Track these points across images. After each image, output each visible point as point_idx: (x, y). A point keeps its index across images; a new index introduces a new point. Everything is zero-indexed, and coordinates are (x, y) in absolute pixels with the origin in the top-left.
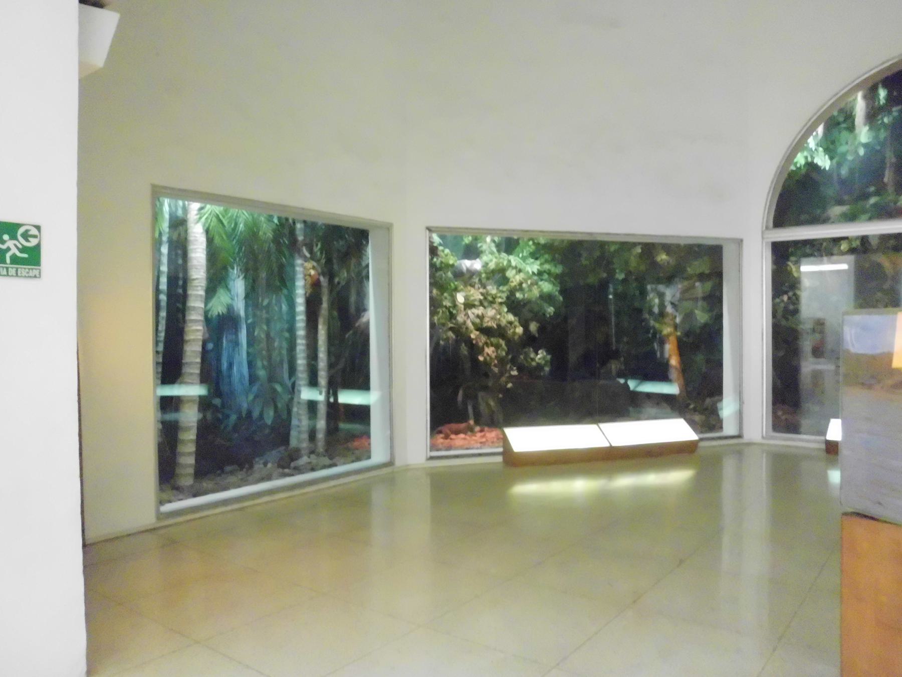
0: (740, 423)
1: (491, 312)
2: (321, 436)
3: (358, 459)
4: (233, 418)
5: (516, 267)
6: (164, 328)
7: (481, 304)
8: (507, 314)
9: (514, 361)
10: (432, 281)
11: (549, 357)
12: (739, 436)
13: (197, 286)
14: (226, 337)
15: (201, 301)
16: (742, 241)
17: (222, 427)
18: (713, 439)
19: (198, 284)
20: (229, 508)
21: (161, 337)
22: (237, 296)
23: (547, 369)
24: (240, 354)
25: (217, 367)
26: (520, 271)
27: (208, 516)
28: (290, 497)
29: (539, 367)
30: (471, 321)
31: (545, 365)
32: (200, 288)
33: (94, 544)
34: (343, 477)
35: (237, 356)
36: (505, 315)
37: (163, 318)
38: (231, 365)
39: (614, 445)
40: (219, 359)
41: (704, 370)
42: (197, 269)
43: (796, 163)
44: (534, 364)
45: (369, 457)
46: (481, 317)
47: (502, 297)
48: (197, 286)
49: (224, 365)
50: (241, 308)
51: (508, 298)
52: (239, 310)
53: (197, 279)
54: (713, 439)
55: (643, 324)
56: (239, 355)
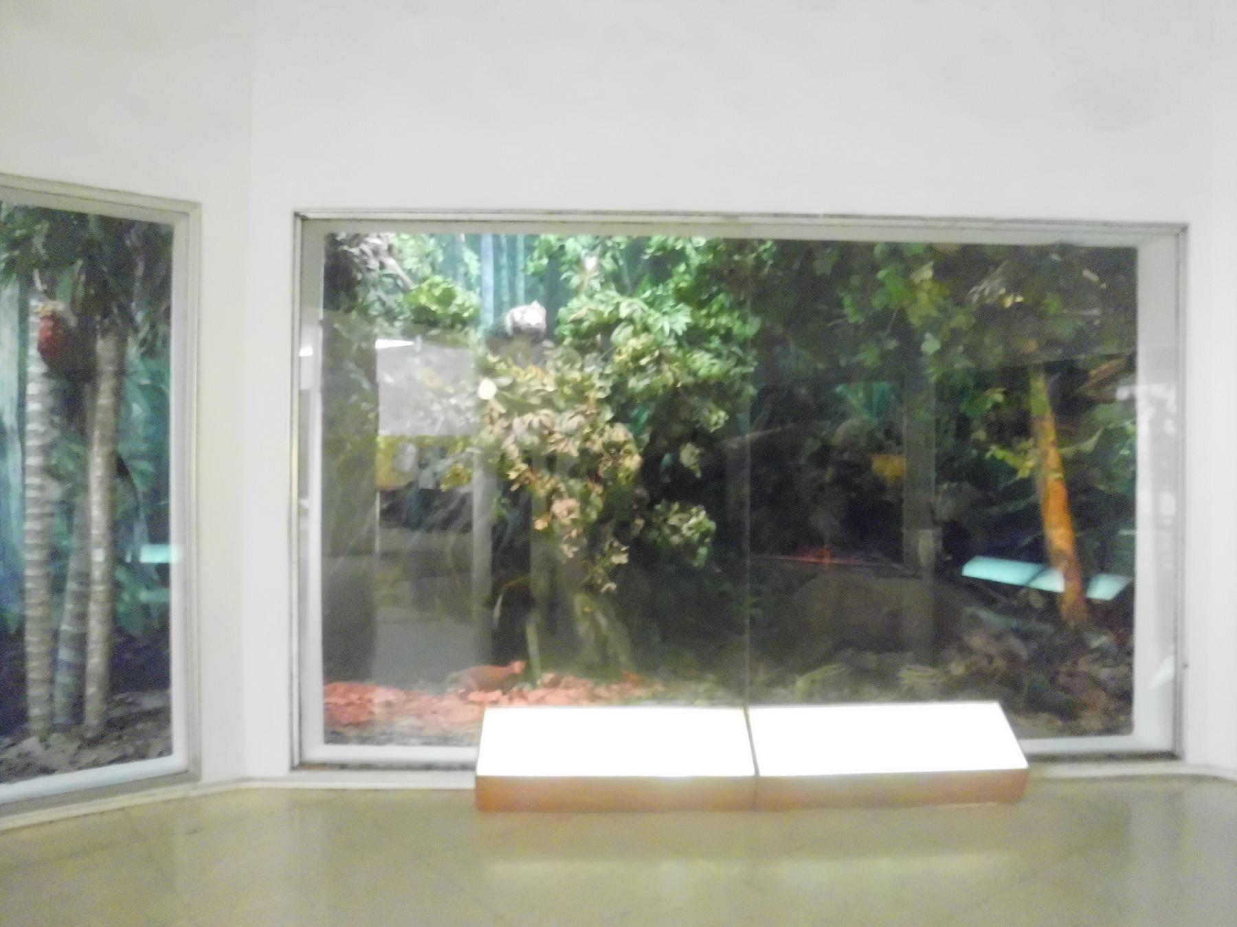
0: (1175, 705)
1: (569, 421)
2: (919, 674)
3: (141, 755)
5: (630, 320)
7: (548, 402)
8: (612, 426)
9: (622, 531)
10: (823, 266)
11: (712, 525)
12: (1170, 756)
16: (1184, 229)
18: (1112, 757)
23: (703, 551)
26: (646, 329)
29: (689, 548)
30: (516, 442)
31: (701, 542)
36: (607, 427)
39: (763, 773)
43: (12, 429)
44: (675, 539)
46: (545, 433)
47: (600, 388)
51: (615, 388)
54: (1112, 757)
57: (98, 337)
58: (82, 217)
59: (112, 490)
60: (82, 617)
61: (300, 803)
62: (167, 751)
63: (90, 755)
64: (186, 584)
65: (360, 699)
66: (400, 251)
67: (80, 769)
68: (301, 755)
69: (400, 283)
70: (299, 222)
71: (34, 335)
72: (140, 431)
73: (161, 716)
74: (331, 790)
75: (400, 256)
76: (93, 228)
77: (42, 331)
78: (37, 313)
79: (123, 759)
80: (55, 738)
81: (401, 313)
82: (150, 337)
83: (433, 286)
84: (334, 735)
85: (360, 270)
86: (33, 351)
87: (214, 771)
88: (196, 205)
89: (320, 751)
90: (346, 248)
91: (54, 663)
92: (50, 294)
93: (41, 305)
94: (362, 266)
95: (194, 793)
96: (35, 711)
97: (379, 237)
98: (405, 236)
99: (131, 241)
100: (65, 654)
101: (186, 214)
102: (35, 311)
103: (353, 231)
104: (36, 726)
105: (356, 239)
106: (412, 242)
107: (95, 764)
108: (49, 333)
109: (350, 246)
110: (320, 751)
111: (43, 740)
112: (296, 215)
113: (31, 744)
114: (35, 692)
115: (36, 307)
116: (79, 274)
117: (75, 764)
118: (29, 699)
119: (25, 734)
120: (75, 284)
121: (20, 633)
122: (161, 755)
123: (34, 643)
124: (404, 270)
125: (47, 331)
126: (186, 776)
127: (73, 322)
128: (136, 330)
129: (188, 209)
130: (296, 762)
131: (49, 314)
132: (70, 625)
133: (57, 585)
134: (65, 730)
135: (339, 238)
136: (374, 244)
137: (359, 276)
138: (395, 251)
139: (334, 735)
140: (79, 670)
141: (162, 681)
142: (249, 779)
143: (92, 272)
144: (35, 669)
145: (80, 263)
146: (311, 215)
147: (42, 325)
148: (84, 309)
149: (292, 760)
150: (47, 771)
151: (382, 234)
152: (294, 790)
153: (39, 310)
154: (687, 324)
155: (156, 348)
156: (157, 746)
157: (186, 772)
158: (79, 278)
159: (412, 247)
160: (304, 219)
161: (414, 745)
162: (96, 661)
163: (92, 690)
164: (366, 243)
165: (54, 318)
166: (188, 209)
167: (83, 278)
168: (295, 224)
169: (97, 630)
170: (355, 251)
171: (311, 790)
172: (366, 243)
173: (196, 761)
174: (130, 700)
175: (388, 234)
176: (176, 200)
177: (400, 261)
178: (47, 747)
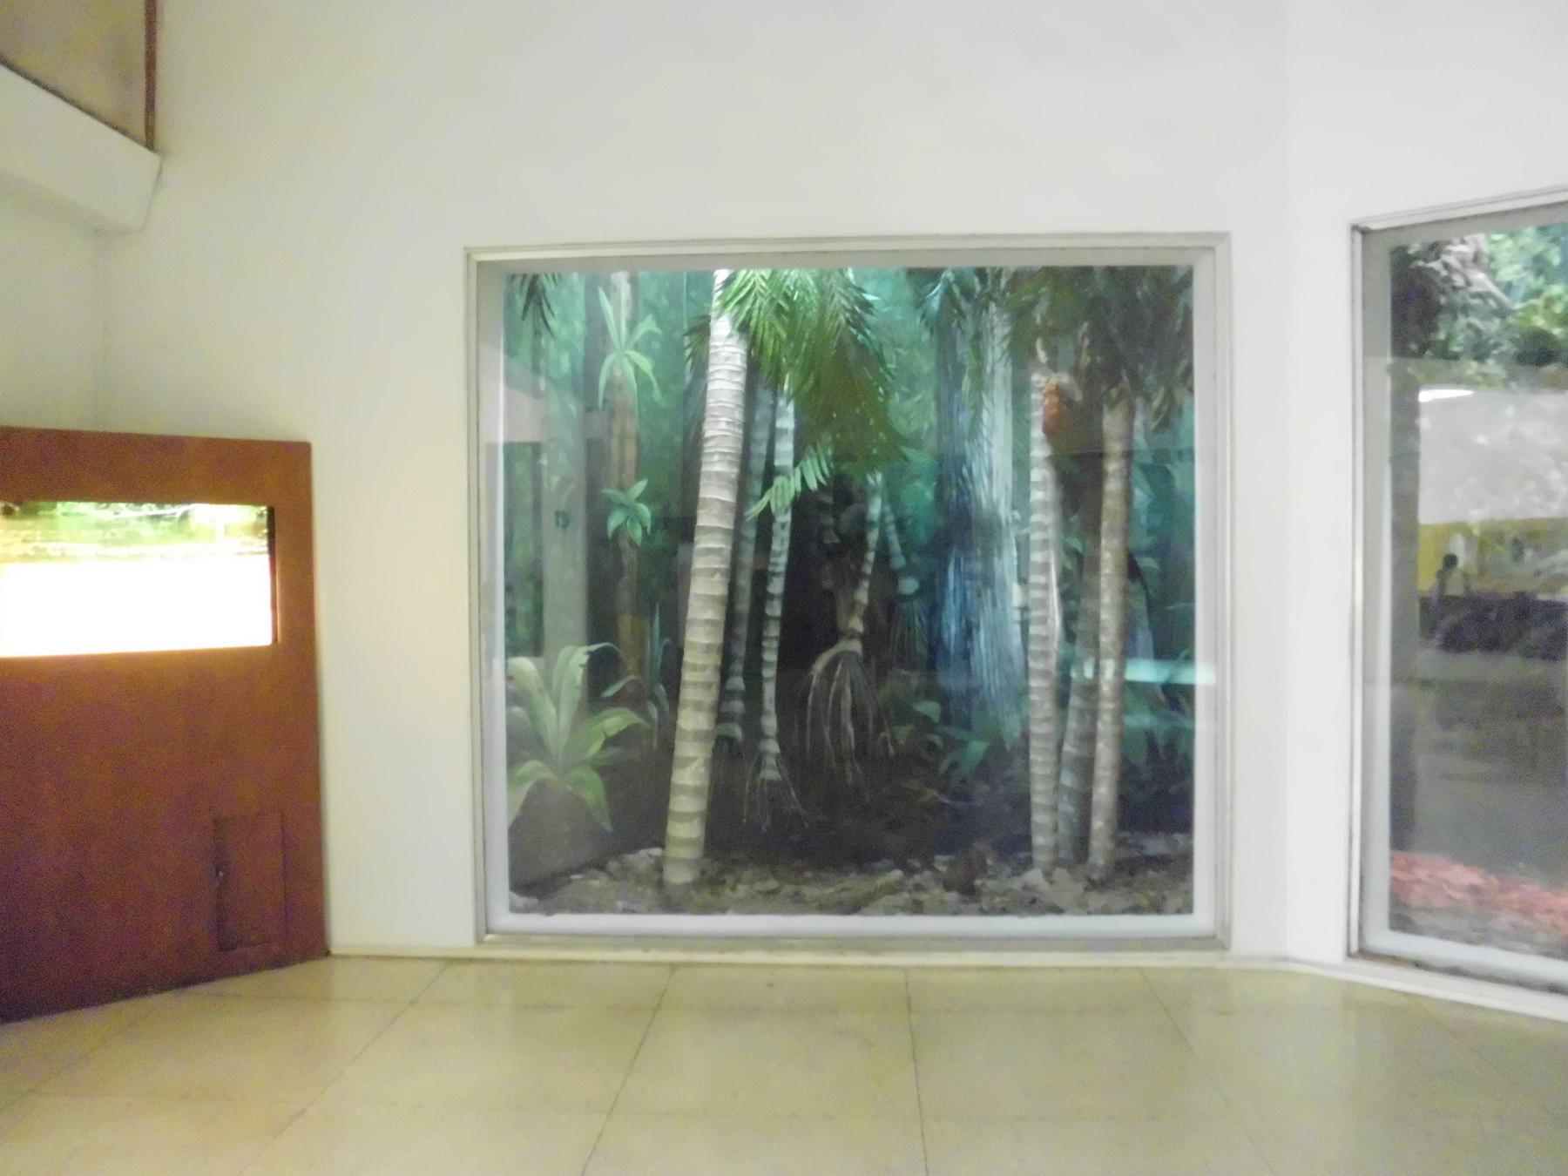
3: (1157, 908)
4: (978, 748)
6: (786, 545)
13: (712, 454)
14: (957, 565)
15: (721, 487)
17: (944, 765)
19: (713, 450)
20: (652, 956)
21: (776, 564)
22: (990, 475)
24: (999, 606)
25: (930, 629)
27: (699, 965)
28: (828, 967)
32: (716, 458)
33: (344, 957)
34: (1059, 949)
35: (988, 608)
37: (783, 526)
38: (969, 632)
40: (934, 611)
41: (828, 568)
42: (713, 416)
45: (1186, 908)
48: (712, 454)
49: (949, 627)
50: (1003, 501)
52: (994, 506)
53: (713, 437)
54: (1147, 944)
55: (1414, 347)
56: (994, 605)
57: (1105, 410)
58: (1086, 271)
59: (1125, 592)
60: (1090, 738)
61: (1356, 1002)
62: (1186, 908)
63: (1095, 899)
64: (1217, 712)
65: (1430, 876)
66: (1492, 259)
67: (1089, 913)
68: (1361, 936)
69: (1492, 303)
70: (1358, 237)
71: (1038, 414)
72: (1143, 519)
73: (1180, 866)
74: (1405, 994)
75: (1493, 266)
76: (1100, 283)
77: (1046, 409)
78: (1041, 389)
79: (1136, 910)
80: (1060, 874)
81: (1496, 345)
82: (1165, 408)
83: (1550, 302)
84: (1401, 920)
85: (1443, 292)
86: (1037, 433)
87: (1248, 940)
88: (1223, 236)
89: (1386, 939)
90: (1421, 263)
91: (1057, 788)
92: (1053, 366)
93: (1044, 379)
94: (1447, 286)
95: (1220, 965)
96: (1039, 840)
97: (1463, 242)
98: (1497, 237)
99: (1143, 290)
100: (1067, 780)
101: (1211, 249)
102: (1039, 386)
103: (1431, 239)
104: (1041, 857)
105: (1435, 249)
106: (1509, 243)
107: (1106, 911)
108: (1054, 411)
109: (1426, 261)
110: (1386, 939)
111: (1048, 875)
112: (1355, 228)
113: (1034, 876)
114: (1040, 818)
115: (1039, 382)
116: (1083, 338)
117: (1083, 908)
118: (1033, 826)
119: (1028, 864)
120: (1078, 353)
121: (1025, 752)
122: (1179, 911)
123: (1040, 763)
124: (1497, 285)
125: (1052, 409)
126: (1215, 941)
127: (1078, 396)
128: (1148, 399)
129: (1211, 244)
130: (1354, 948)
131: (1053, 388)
132: (1074, 746)
133: (1062, 701)
134: (1069, 866)
135: (1411, 252)
136: (1460, 252)
137: (1443, 300)
138: (1485, 260)
139: (1401, 920)
140: (1085, 801)
141: (1185, 824)
142: (1286, 959)
143: (1098, 330)
144: (1040, 794)
145: (1085, 326)
146: (1374, 226)
147: (1047, 402)
148: (1088, 378)
149: (1349, 947)
150: (1057, 910)
151: (1466, 238)
152: (1351, 985)
153: (1042, 385)
154: (653, 319)
155: (1171, 418)
156: (1174, 901)
157: (1214, 937)
158: (1083, 342)
159: (1508, 250)
160: (1365, 232)
161: (1525, 952)
162: (1104, 792)
163: (1098, 824)
164: (1449, 253)
165: (1059, 391)
166: (1211, 244)
167: (1087, 342)
168: (1353, 241)
169: (1106, 754)
170: (1436, 265)
171: (823, 908)
172: (1449, 253)
173: (1225, 926)
174: (1130, 841)
175: (1477, 236)
176: (1140, 234)
177: (1492, 273)
178: (1052, 883)
